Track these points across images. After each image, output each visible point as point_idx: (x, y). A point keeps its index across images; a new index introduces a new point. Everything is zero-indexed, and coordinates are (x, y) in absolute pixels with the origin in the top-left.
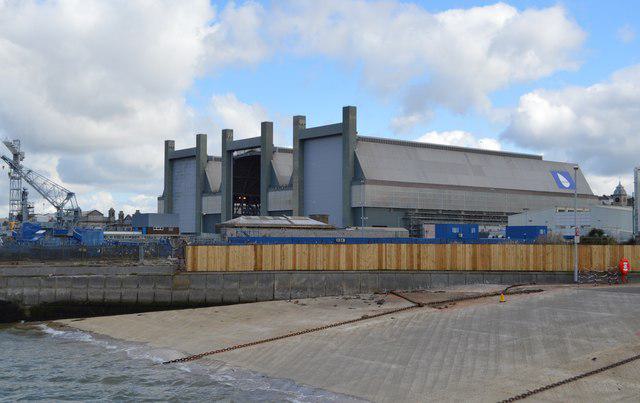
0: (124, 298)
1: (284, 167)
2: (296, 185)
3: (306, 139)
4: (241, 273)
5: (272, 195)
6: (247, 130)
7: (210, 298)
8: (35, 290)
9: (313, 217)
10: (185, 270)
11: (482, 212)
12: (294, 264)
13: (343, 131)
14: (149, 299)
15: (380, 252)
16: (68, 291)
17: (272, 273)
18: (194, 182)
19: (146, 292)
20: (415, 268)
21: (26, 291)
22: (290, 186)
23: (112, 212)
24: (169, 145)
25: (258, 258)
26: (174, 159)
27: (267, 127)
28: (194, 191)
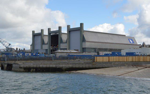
0: (83, 67)
1: (64, 38)
2: (68, 42)
3: (70, 31)
4: (106, 62)
5: (61, 44)
6: (55, 29)
7: (100, 67)
8: (65, 66)
9: (75, 50)
10: (95, 61)
11: (112, 49)
12: (116, 60)
13: (80, 29)
14: (88, 67)
15: (132, 58)
16: (72, 66)
17: (112, 62)
18: (40, 41)
19: (87, 66)
20: (139, 61)
21: (63, 66)
22: (66, 42)
23: (17, 49)
24: (33, 32)
25: (109, 59)
26: (35, 35)
27: (60, 28)
28: (40, 43)
